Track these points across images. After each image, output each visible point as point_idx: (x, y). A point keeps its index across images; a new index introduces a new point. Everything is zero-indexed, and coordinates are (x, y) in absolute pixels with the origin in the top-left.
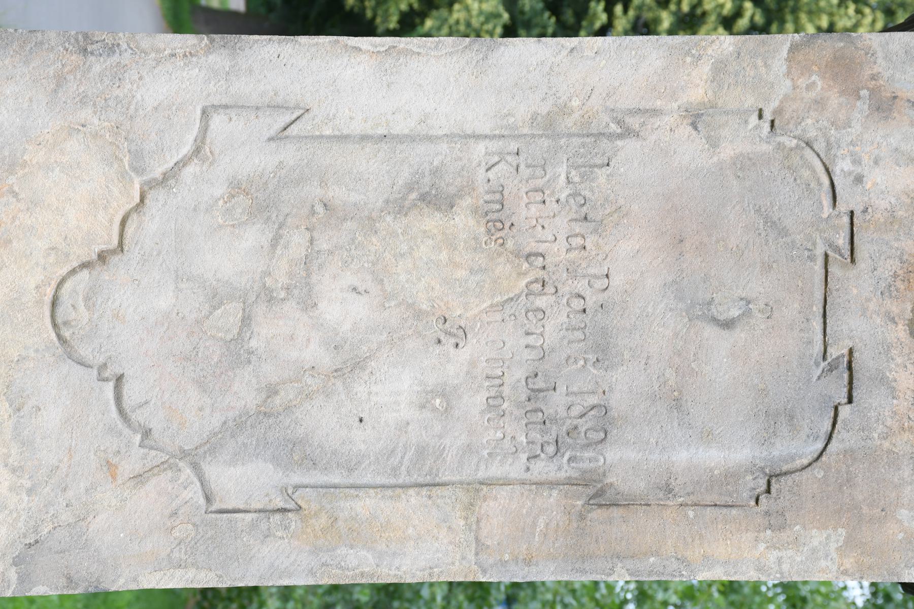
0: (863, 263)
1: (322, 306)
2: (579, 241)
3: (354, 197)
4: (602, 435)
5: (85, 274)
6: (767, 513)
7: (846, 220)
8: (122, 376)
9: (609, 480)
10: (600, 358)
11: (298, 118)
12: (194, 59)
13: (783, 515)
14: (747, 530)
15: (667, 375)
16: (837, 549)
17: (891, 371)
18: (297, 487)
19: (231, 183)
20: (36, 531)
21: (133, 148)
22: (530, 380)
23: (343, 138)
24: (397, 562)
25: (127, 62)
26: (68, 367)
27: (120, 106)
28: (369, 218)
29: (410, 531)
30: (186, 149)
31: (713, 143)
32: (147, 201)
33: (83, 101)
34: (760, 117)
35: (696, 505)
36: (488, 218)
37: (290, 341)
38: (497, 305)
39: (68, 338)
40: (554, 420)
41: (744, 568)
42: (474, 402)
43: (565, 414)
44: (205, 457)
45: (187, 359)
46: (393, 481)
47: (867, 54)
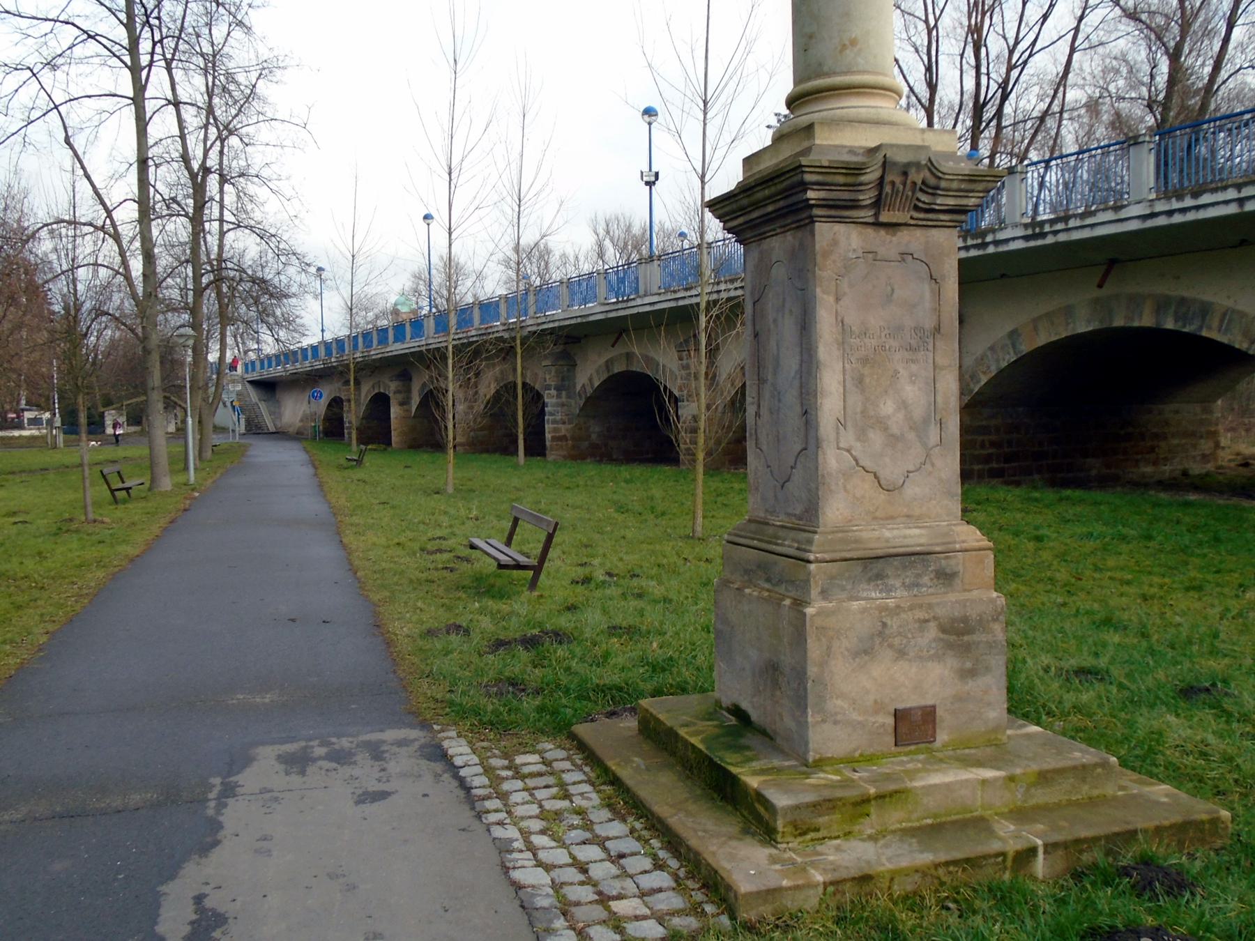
42: (914, 367)
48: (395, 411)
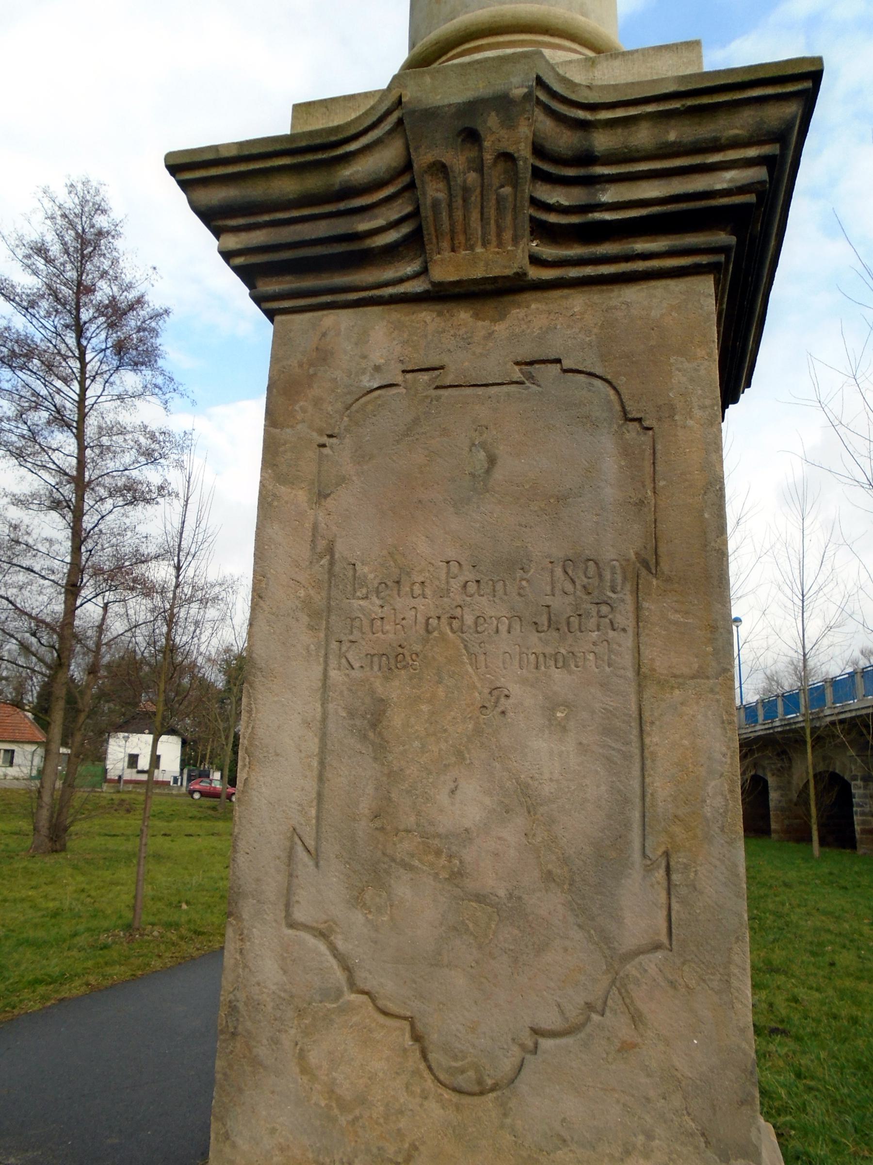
0: (445, 359)
1: (467, 824)
2: (417, 589)
3: (370, 790)
4: (591, 563)
5: (431, 1056)
6: (659, 419)
7: (409, 376)
8: (532, 1029)
9: (633, 556)
10: (520, 566)
11: (300, 838)
12: (245, 932)
13: (660, 407)
14: (676, 435)
15: (536, 508)
16: (688, 362)
17: (533, 332)
18: (644, 855)
19: (353, 906)
20: (692, 1135)
21: (318, 998)
22: (540, 629)
23: (320, 795)
24: (717, 756)
25: (244, 995)
26: (522, 1086)
27: (281, 1007)
28: (389, 775)
29: (686, 742)
30: (323, 947)
31: (342, 480)
32: (366, 989)
33: (275, 1041)
34: (324, 446)
35: (654, 480)
36: (393, 668)
37: (498, 856)
38: (471, 659)
39: (493, 1081)
40: (577, 607)
41: (711, 436)
42: (561, 680)
43: (571, 597)
44: (614, 949)
45: (516, 960)
46: (637, 759)
47: (283, 372)
48: (774, 796)
